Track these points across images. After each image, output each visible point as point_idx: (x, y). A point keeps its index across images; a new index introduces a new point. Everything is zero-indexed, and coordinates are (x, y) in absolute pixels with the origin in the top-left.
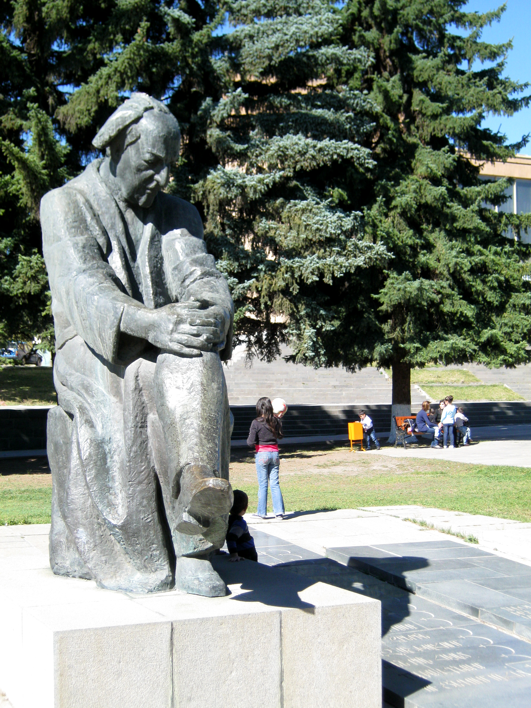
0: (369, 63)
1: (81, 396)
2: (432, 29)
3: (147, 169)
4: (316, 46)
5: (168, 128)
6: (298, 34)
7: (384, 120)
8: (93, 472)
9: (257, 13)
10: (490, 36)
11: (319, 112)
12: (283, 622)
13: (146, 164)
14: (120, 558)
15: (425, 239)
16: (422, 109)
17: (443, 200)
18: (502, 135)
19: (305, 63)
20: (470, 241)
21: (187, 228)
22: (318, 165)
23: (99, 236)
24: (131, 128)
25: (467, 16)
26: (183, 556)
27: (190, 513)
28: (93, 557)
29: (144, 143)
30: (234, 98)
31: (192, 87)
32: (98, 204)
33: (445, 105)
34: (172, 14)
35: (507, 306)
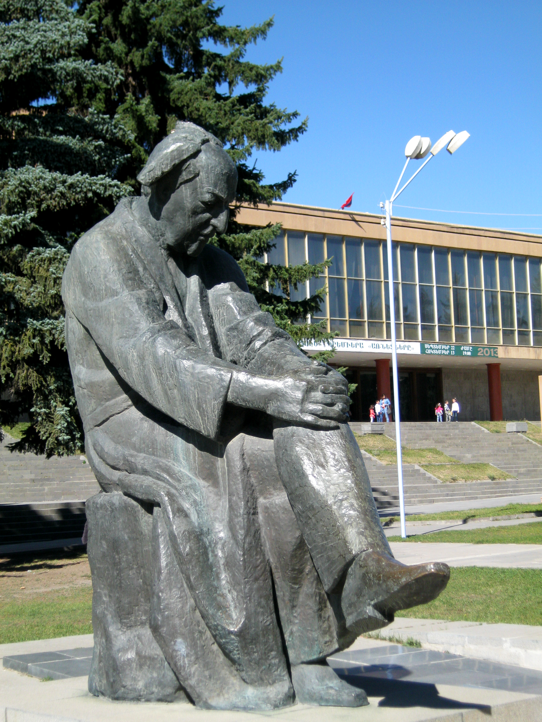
0: (118, 81)
1: (161, 480)
3: (203, 212)
5: (229, 164)
7: (137, 151)
8: (197, 570)
10: (255, 55)
11: (62, 139)
14: (223, 672)
18: (258, 172)
19: (40, 77)
22: (68, 204)
25: (228, 31)
26: (303, 663)
27: (376, 607)
28: (194, 673)
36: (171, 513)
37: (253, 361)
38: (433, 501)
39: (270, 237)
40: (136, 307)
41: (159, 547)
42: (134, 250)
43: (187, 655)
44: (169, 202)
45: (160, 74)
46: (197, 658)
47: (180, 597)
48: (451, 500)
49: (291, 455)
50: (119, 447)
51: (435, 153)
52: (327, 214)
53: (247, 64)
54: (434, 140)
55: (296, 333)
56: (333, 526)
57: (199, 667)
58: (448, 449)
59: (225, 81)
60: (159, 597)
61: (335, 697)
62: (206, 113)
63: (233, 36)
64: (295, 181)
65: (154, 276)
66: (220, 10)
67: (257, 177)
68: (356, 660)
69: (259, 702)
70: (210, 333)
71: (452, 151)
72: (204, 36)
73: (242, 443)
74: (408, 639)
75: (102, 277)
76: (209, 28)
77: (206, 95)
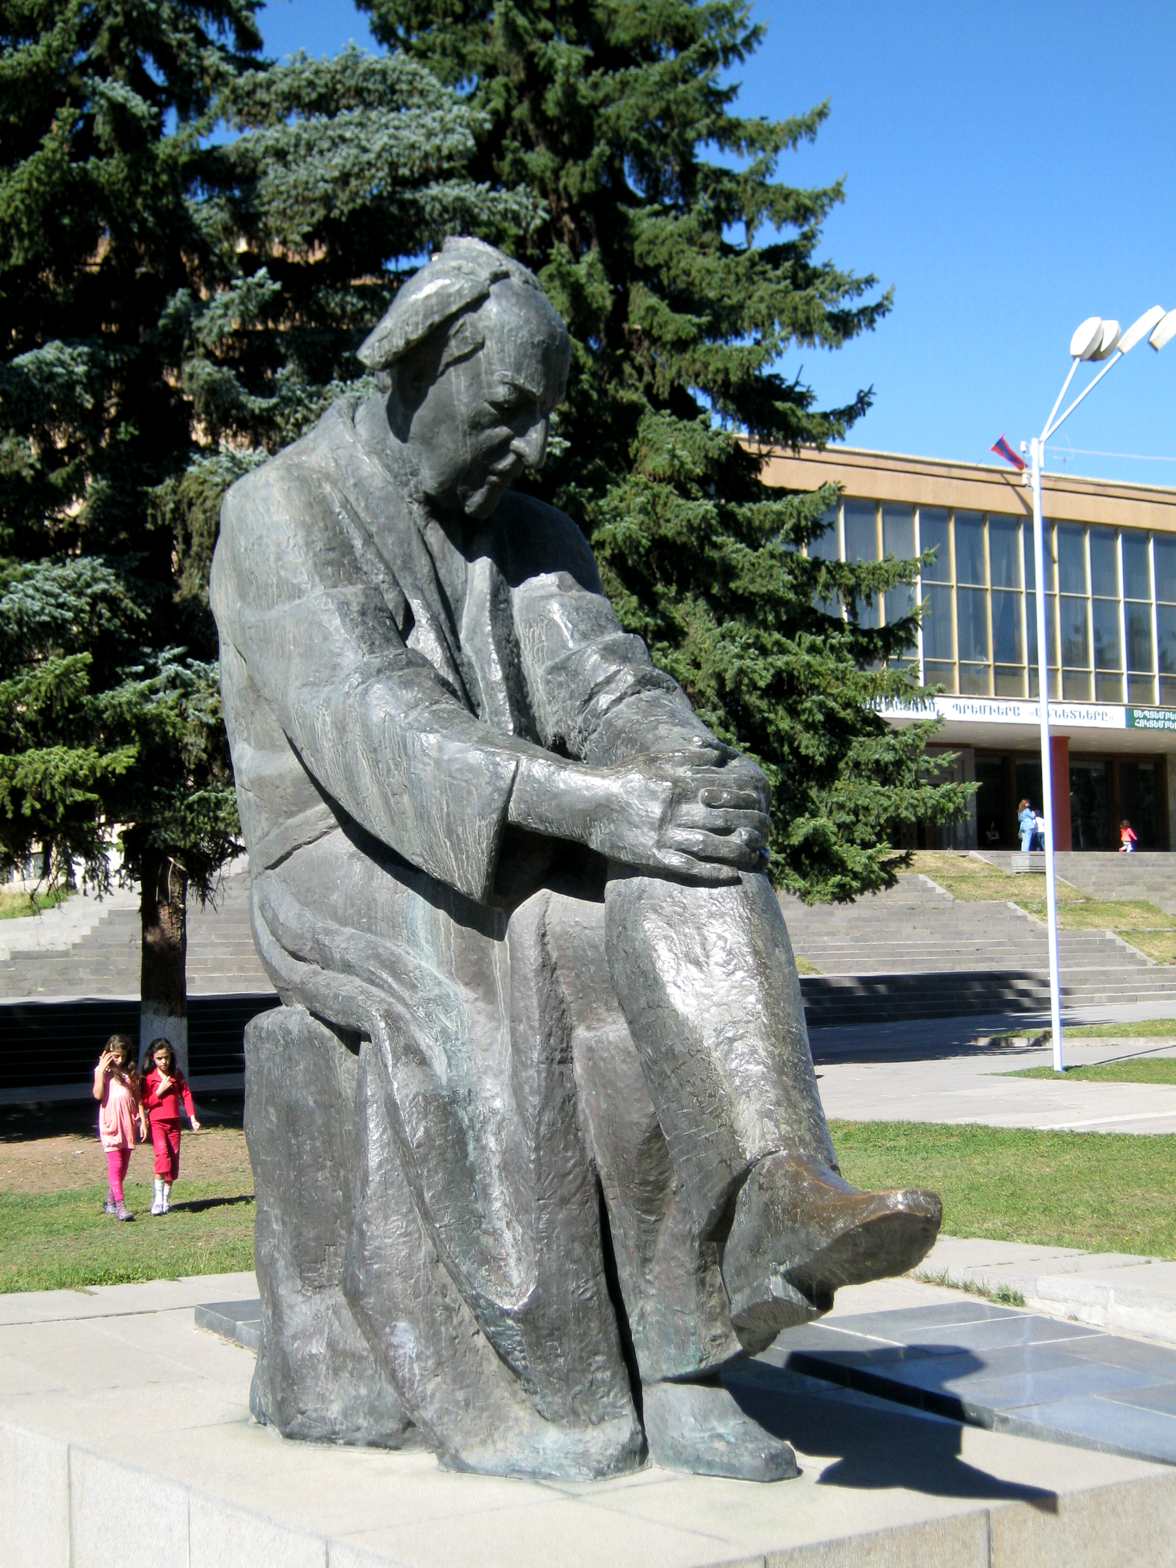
0: (538, 222)
2: (669, 151)
3: (494, 424)
4: (422, 180)
5: (549, 324)
6: (395, 150)
9: (292, 100)
10: (795, 171)
12: (994, 1536)
13: (493, 410)
14: (497, 1393)
15: (665, 617)
16: (651, 327)
17: (703, 532)
18: (804, 390)
19: (394, 216)
20: (765, 620)
21: (571, 572)
23: (385, 586)
24: (461, 322)
26: (666, 1380)
27: (791, 1277)
28: (433, 1395)
29: (495, 360)
30: (249, 290)
31: (139, 265)
32: (367, 507)
33: (704, 319)
34: (110, 94)
35: (842, 765)
36: (390, 1057)
37: (595, 736)
38: (1135, 999)
39: (817, 509)
40: (337, 621)
41: (366, 1127)
42: (345, 503)
43: (418, 1357)
44: (425, 403)
45: (616, 210)
46: (439, 1364)
47: (406, 1234)
48: (1169, 997)
49: (633, 940)
50: (308, 914)
51: (1126, 349)
52: (956, 472)
53: (780, 189)
54: (1125, 326)
55: (865, 687)
56: (710, 1096)
57: (444, 1382)
58: (1171, 903)
59: (740, 219)
60: (362, 1234)
61: (725, 1459)
62: (702, 279)
63: (754, 136)
64: (870, 404)
65: (386, 556)
66: (733, 89)
67: (802, 399)
68: (882, 1333)
69: (565, 1462)
70: (506, 678)
71: (1158, 344)
72: (699, 137)
73: (545, 910)
74: (1000, 1289)
75: (272, 558)
76: (707, 121)
77: (703, 246)
